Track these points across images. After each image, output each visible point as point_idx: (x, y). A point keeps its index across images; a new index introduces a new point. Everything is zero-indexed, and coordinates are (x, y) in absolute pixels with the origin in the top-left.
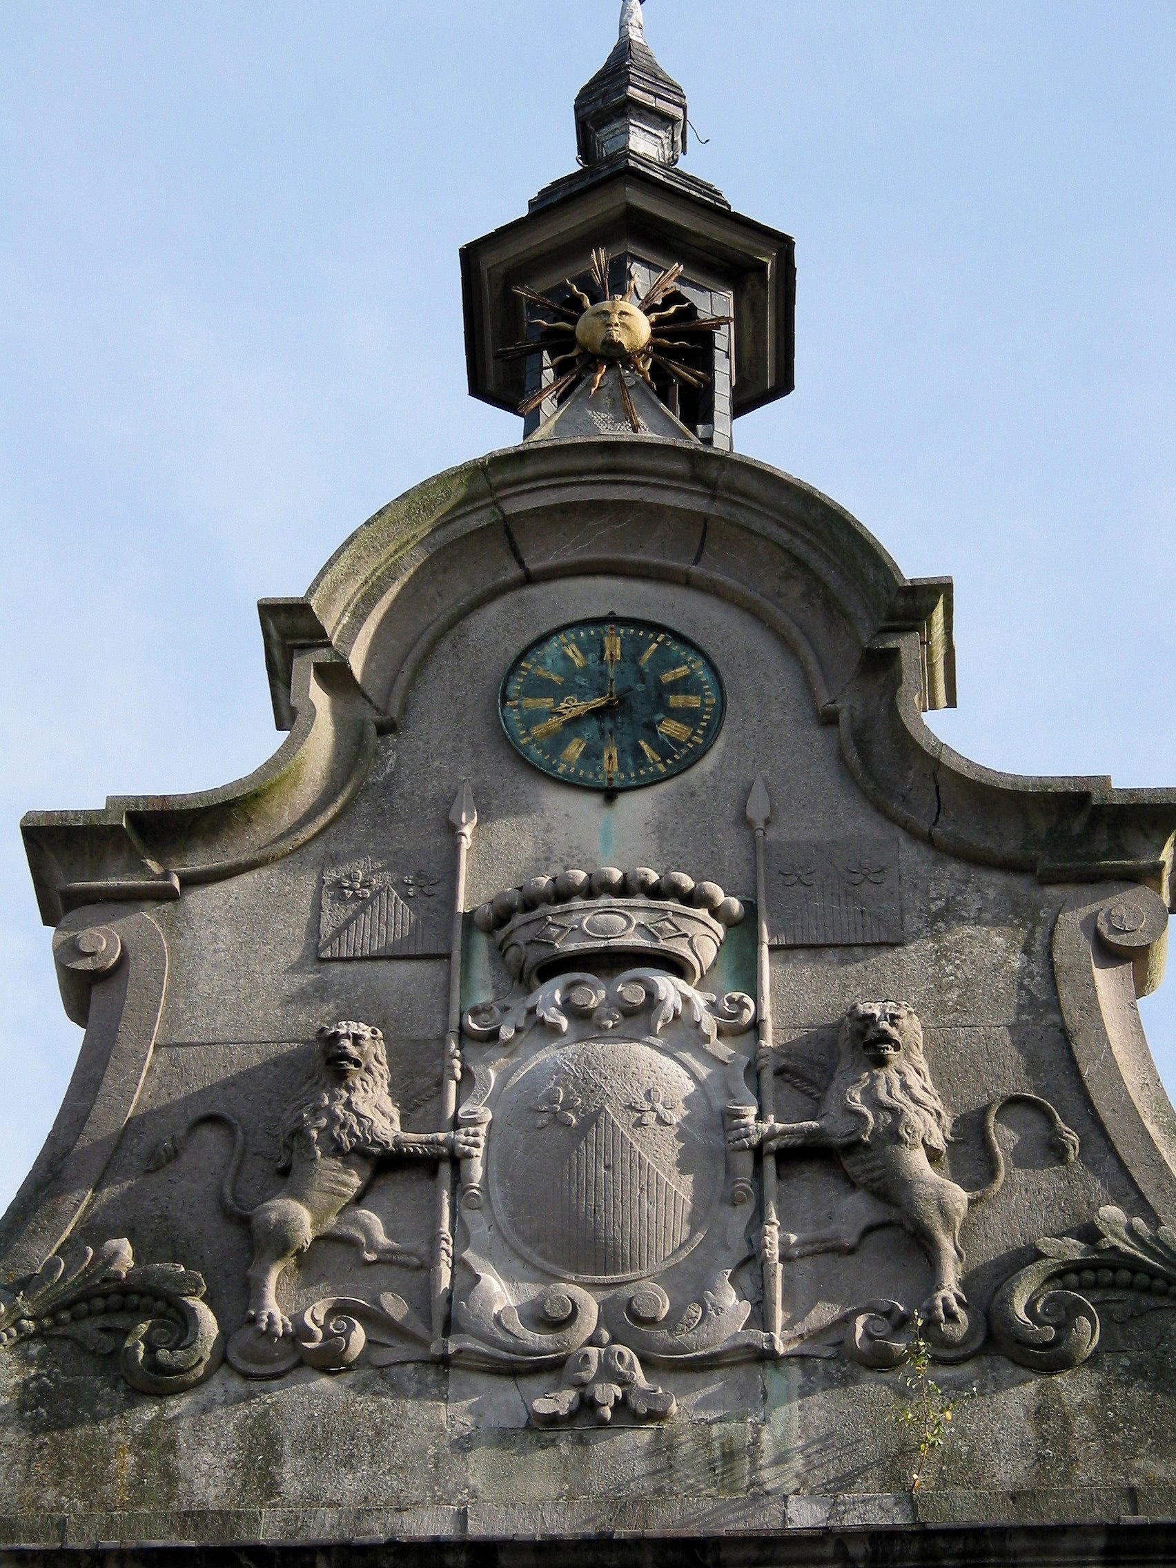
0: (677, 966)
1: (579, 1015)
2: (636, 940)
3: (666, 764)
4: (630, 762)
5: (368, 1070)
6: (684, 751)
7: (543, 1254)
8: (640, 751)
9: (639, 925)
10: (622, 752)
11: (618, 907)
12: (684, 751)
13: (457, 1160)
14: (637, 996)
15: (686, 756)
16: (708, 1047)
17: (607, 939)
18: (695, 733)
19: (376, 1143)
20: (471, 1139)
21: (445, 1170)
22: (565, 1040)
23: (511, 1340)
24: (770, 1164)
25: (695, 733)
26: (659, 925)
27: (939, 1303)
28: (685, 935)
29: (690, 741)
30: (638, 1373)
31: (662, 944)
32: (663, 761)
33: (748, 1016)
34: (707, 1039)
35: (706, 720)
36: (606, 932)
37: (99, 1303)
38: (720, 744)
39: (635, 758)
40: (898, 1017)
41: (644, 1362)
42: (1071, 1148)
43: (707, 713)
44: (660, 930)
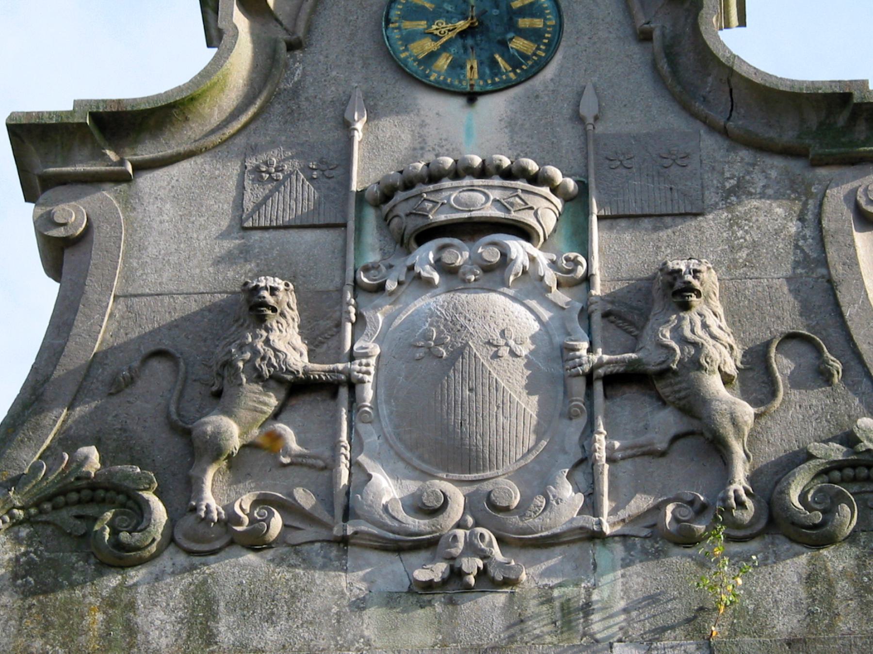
0: (524, 232)
1: (448, 271)
2: (492, 212)
3: (515, 73)
4: (487, 71)
5: (282, 315)
6: (530, 63)
7: (421, 458)
8: (496, 63)
9: (495, 201)
10: (480, 63)
11: (479, 186)
12: (530, 63)
13: (353, 385)
14: (493, 256)
15: (532, 66)
16: (550, 296)
17: (470, 211)
18: (538, 49)
19: (288, 372)
20: (364, 368)
21: (344, 392)
22: (437, 291)
23: (396, 524)
24: (599, 387)
25: (538, 49)
26: (511, 200)
27: (731, 494)
28: (531, 208)
29: (534, 54)
30: (496, 550)
31: (514, 215)
32: (514, 71)
33: (581, 271)
34: (549, 289)
35: (547, 38)
36: (469, 206)
37: (74, 496)
38: (558, 57)
39: (491, 69)
40: (699, 271)
41: (501, 541)
42: (835, 373)
43: (548, 32)
44: (512, 204)
